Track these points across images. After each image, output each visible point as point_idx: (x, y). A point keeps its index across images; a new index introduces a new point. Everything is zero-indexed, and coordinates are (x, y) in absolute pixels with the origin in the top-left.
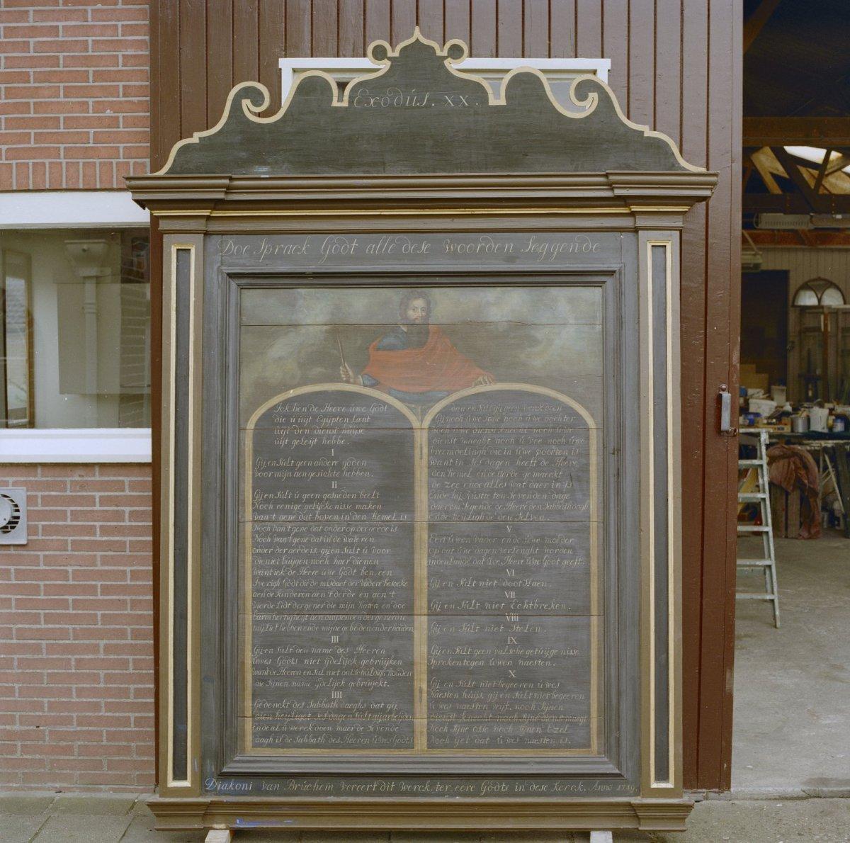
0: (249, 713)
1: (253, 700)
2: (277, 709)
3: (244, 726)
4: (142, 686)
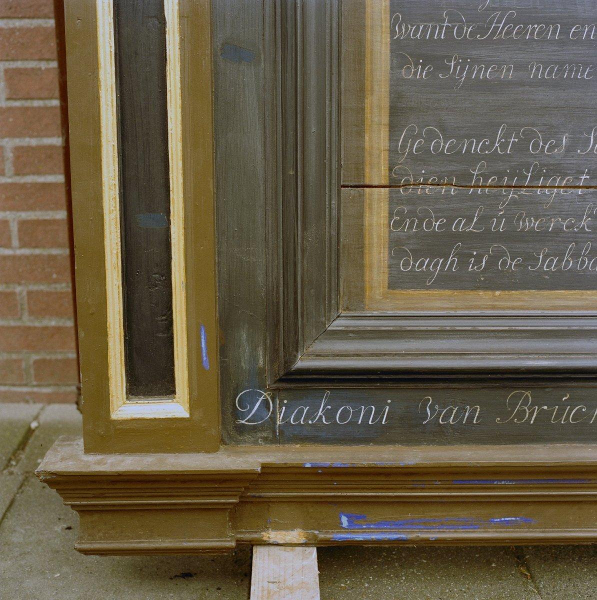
0: (377, 172)
1: (394, 129)
2: (476, 159)
3: (361, 216)
4: (34, 142)
